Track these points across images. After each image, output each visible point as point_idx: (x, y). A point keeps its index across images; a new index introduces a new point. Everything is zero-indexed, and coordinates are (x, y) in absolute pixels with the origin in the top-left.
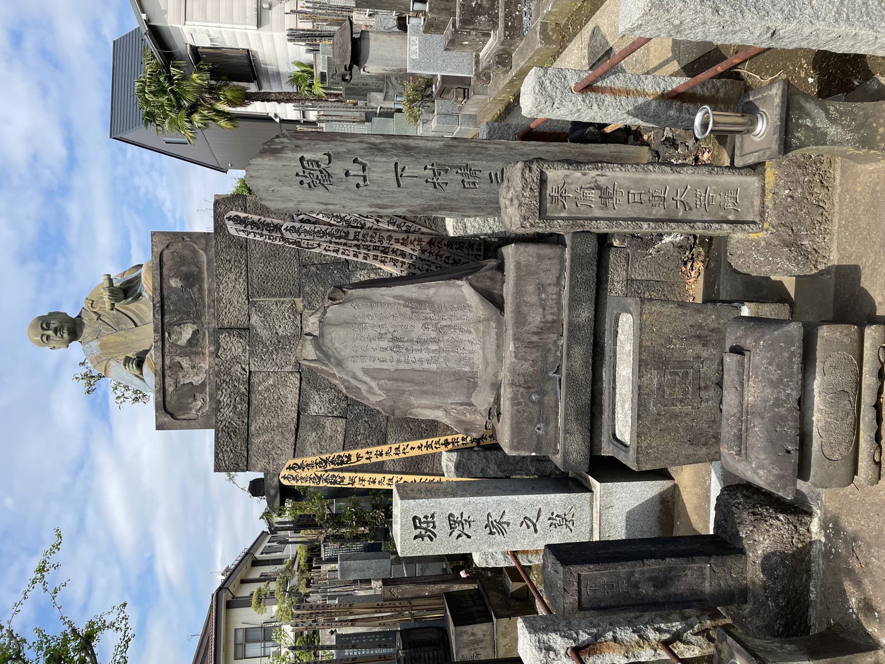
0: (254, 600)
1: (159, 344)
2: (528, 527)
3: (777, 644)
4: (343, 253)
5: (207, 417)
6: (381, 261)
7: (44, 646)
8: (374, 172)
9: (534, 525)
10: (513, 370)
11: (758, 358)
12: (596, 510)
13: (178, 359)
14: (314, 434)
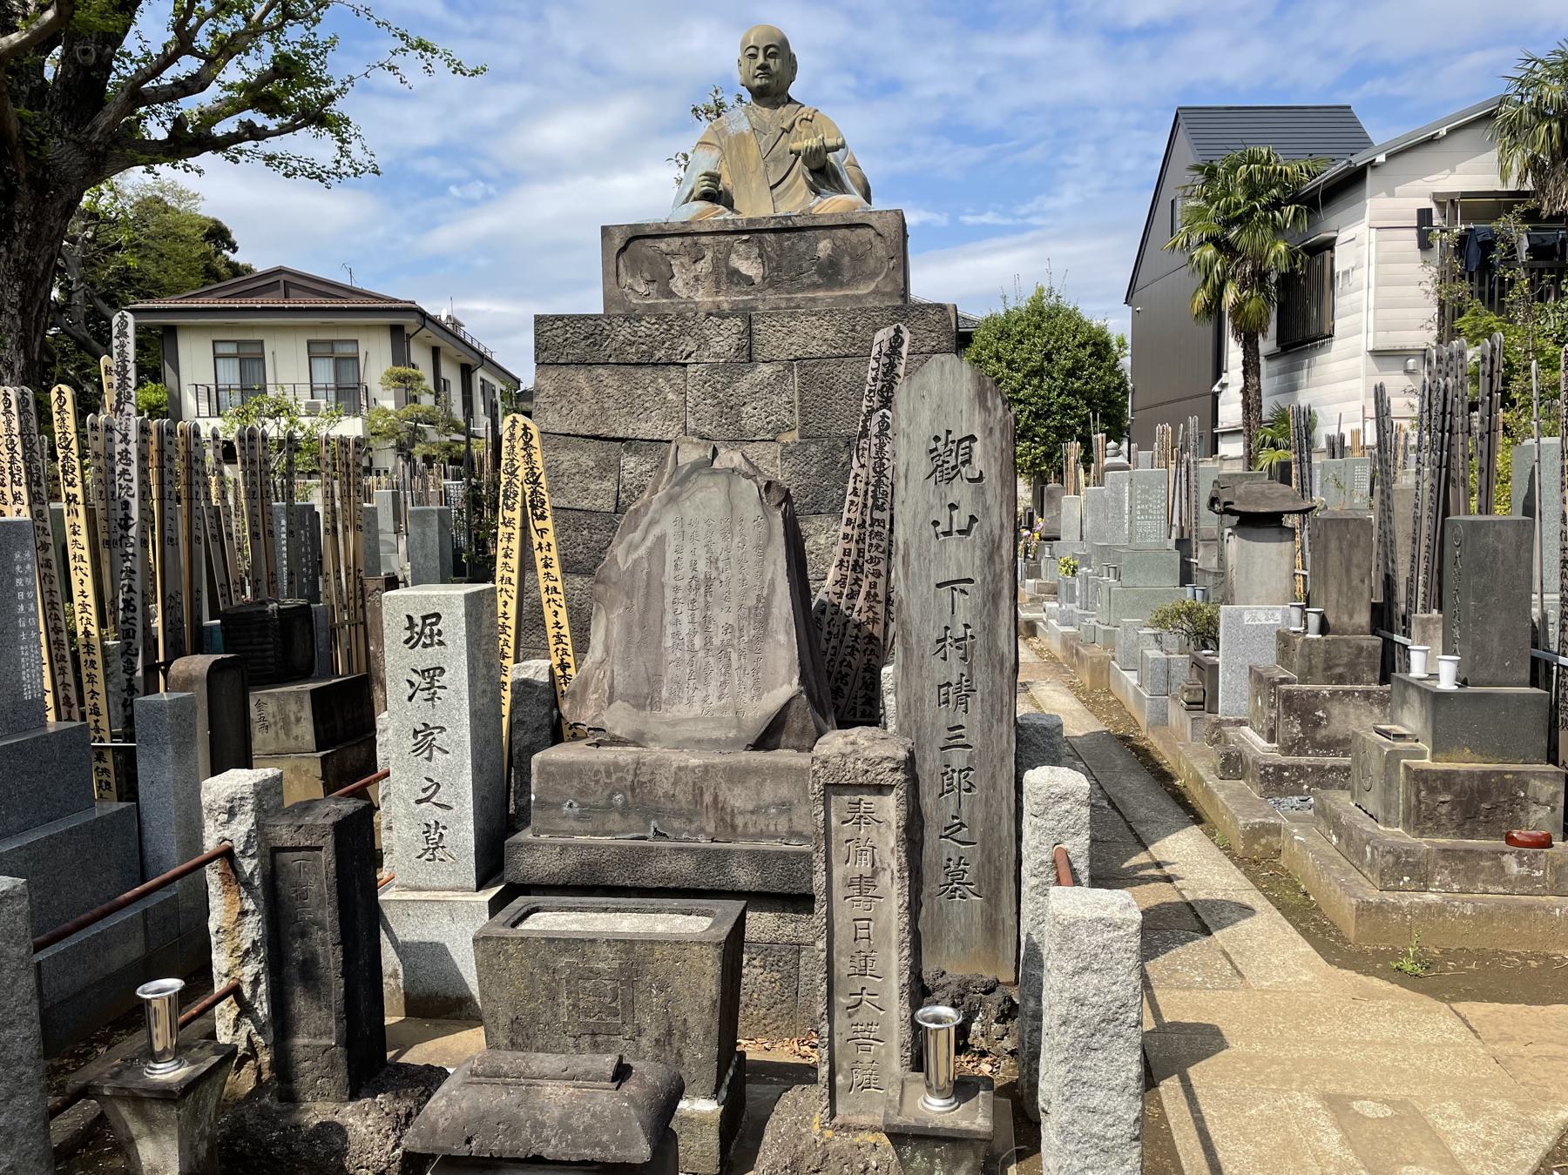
0: (403, 370)
1: (731, 227)
2: (424, 790)
3: (208, 1130)
4: (852, 502)
5: (622, 301)
6: (842, 561)
7: (309, 51)
8: (958, 546)
9: (427, 800)
10: (659, 764)
11: (607, 1099)
12: (449, 896)
13: (709, 255)
14: (592, 464)
